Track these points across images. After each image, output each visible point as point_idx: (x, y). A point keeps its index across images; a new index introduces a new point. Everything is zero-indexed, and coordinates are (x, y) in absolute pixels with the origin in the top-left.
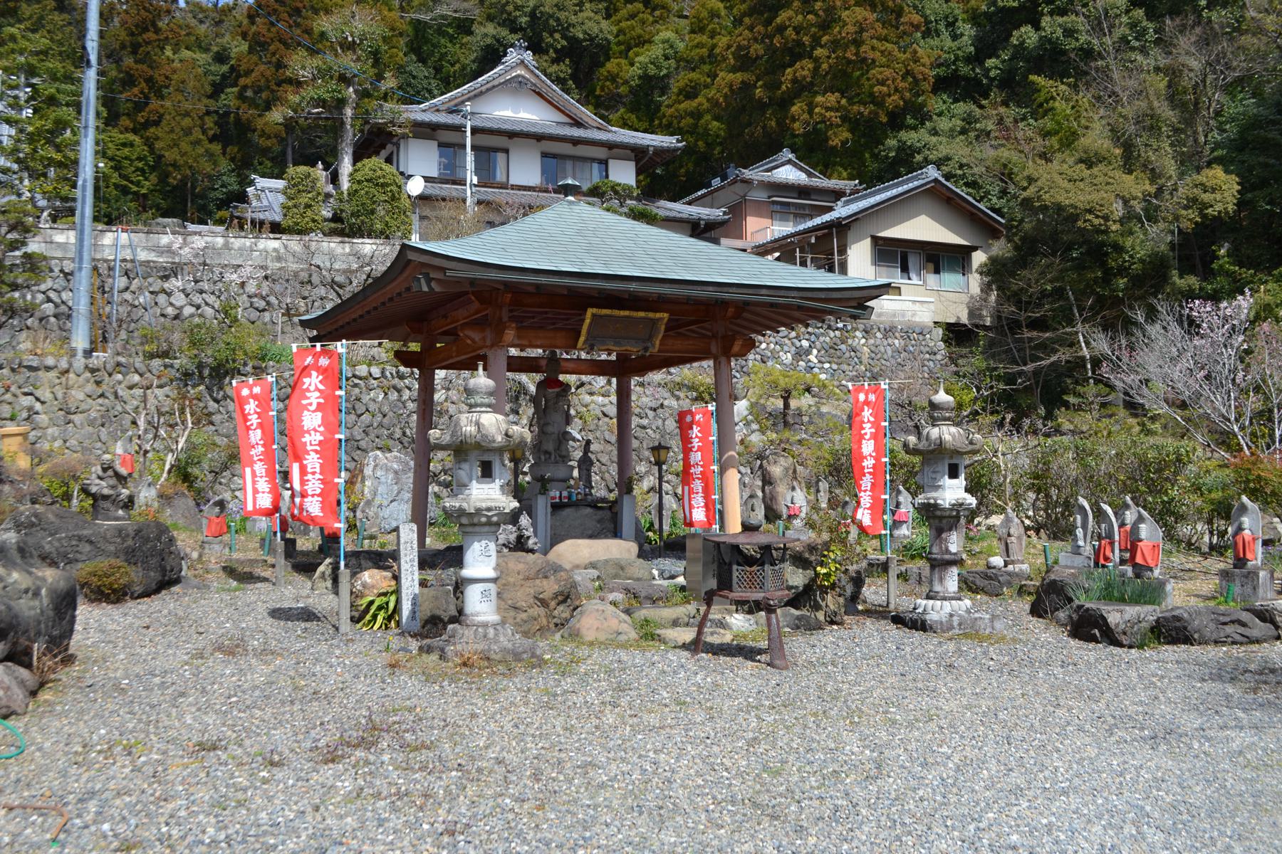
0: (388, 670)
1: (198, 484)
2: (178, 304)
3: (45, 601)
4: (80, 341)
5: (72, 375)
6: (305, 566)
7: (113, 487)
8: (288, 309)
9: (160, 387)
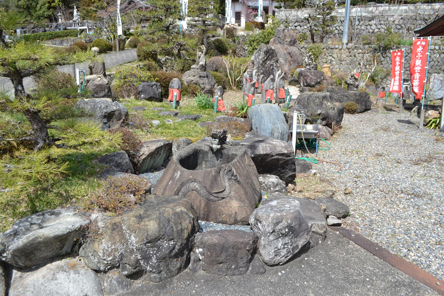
0: (435, 141)
1: (377, 82)
2: (373, 28)
3: (336, 111)
4: (345, 40)
5: (342, 50)
6: (408, 108)
7: (354, 82)
8: (408, 28)
9: (367, 53)
